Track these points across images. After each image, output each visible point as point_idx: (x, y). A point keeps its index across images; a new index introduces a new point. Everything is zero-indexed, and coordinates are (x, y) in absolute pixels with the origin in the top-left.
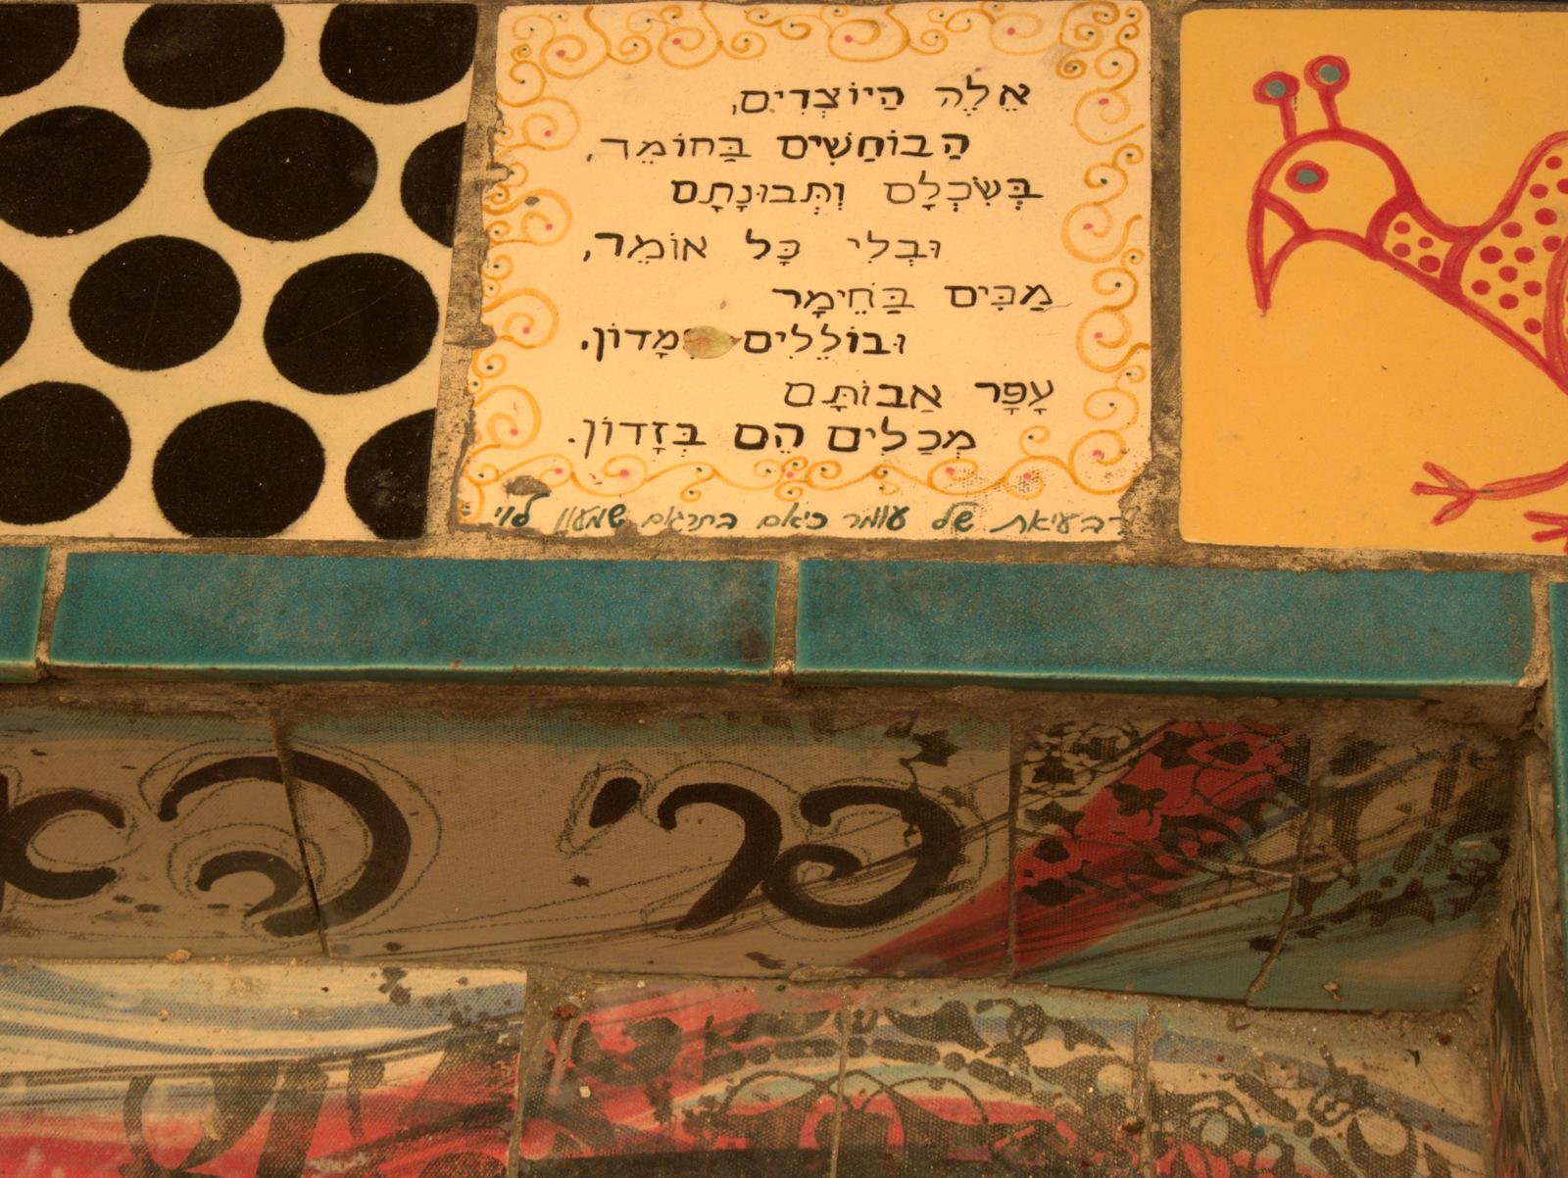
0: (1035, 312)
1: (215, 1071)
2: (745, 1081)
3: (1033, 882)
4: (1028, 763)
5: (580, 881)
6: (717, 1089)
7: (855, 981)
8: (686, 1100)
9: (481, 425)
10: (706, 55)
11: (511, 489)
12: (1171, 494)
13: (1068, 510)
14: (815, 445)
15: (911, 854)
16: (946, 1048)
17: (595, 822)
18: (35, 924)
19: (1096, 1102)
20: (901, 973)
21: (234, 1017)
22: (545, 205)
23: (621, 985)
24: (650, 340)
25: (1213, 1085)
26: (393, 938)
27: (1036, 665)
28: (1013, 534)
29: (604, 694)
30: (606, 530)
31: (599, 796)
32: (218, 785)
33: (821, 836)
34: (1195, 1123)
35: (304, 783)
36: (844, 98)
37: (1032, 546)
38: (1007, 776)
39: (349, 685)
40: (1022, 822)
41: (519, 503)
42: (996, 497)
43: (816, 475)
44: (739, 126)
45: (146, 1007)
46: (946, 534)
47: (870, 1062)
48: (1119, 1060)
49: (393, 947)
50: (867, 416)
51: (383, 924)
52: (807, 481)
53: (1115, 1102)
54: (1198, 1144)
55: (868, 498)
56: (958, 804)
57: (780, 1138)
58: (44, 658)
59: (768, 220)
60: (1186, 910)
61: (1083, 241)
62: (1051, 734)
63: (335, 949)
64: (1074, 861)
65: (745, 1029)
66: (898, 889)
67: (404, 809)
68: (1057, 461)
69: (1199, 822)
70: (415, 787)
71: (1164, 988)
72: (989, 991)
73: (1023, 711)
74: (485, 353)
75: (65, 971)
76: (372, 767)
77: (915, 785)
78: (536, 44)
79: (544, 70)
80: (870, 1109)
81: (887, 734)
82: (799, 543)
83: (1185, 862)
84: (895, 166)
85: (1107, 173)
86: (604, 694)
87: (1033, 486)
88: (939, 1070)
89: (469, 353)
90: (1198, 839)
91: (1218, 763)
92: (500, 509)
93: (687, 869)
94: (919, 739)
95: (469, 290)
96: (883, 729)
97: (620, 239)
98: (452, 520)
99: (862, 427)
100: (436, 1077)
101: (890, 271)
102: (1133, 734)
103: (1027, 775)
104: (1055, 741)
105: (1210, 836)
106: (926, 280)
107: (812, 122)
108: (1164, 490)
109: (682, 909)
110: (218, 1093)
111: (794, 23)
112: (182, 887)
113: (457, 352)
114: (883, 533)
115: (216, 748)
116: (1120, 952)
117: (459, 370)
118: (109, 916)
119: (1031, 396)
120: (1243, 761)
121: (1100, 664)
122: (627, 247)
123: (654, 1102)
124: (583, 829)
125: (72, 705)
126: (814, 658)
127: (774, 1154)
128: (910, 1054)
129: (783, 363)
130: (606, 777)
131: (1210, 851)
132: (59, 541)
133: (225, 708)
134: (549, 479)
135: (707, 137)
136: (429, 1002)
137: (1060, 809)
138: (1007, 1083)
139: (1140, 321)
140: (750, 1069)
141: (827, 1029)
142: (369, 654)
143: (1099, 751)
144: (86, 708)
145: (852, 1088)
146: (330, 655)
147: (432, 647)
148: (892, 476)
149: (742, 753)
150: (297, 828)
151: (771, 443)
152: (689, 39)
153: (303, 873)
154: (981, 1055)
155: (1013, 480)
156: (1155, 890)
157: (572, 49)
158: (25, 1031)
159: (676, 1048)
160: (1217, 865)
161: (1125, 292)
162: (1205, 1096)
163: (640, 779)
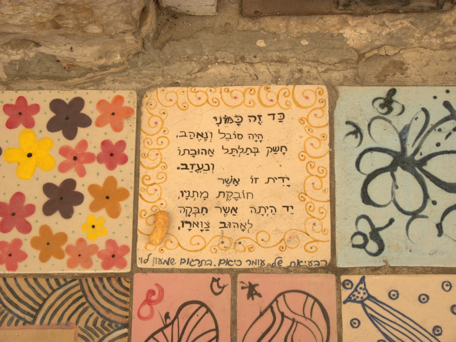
10: (310, 244)
38: (328, 156)
135: (220, 196)
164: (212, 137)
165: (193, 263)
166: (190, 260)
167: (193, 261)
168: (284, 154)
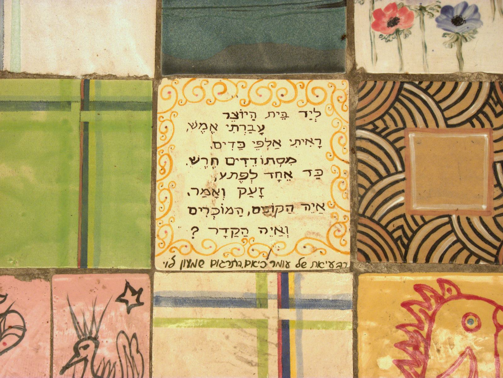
0: (204, 198)
36: (240, 115)
92: (250, 133)
99: (202, 207)
111: (315, 96)
164: (233, 147)
165: (222, 265)
166: (220, 262)
167: (223, 262)
168: (279, 181)
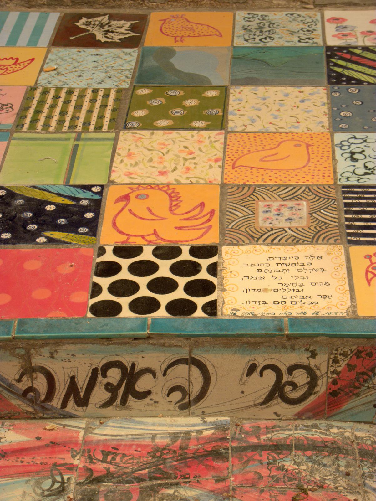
1: (169, 434)
2: (275, 435)
3: (331, 391)
4: (331, 358)
5: (243, 392)
6: (269, 436)
7: (295, 419)
8: (263, 438)
9: (226, 301)
11: (232, 310)
12: (356, 309)
13: (337, 312)
14: (288, 303)
15: (308, 383)
16: (314, 430)
17: (247, 376)
18: (133, 407)
19: (345, 437)
20: (304, 418)
21: (172, 425)
22: (234, 273)
23: (248, 421)
24: (256, 290)
25: (367, 435)
26: (203, 410)
27: (333, 332)
28: (327, 315)
29: (252, 340)
30: (251, 315)
31: (249, 368)
32: (176, 366)
33: (291, 379)
34: (364, 441)
35: (192, 365)
37: (330, 316)
38: (327, 362)
39: (205, 338)
40: (329, 375)
41: (234, 312)
42: (323, 310)
43: (289, 308)
44: (269, 262)
45: (154, 424)
46: (315, 315)
47: (299, 432)
48: (348, 432)
49: (203, 412)
50: (298, 300)
51: (203, 405)
52: (288, 308)
53: (348, 438)
54: (366, 444)
55: (300, 311)
56: (317, 369)
57: (283, 443)
58: (149, 332)
59: (275, 274)
60: (361, 397)
61: (335, 276)
62: (335, 350)
63: (191, 413)
64: (339, 386)
65: (274, 427)
66: (304, 394)
67: (211, 372)
68: (334, 305)
69: (363, 373)
70: (213, 366)
71: (356, 420)
72: (321, 421)
73: (330, 344)
74: (225, 293)
75: (137, 419)
76: (206, 361)
77: (309, 364)
78: (229, 251)
79: (231, 255)
80: (300, 438)
81: (305, 350)
82: (287, 317)
83: (360, 384)
84: (297, 267)
85: (338, 268)
86: (252, 340)
87: (330, 309)
88: (313, 433)
89: (222, 292)
90: (363, 378)
91: (367, 357)
93: (264, 388)
94: (311, 351)
95: (221, 284)
96: (304, 349)
97: (248, 277)
98: (222, 314)
100: (213, 434)
101: (299, 281)
102: (351, 350)
103: (331, 361)
104: (336, 352)
105: (366, 377)
106: (306, 282)
107: (282, 261)
108: (354, 309)
109: (262, 400)
110: (170, 437)
112: (164, 396)
113: (220, 292)
114: (303, 315)
115: (177, 356)
116: (348, 410)
117: (221, 294)
118: (148, 405)
119: (328, 297)
120: (371, 357)
121: (346, 332)
122: (250, 278)
123: (257, 438)
124: (245, 378)
125: (152, 344)
126: (292, 331)
127: (282, 445)
128: (307, 431)
129: (281, 293)
130: (251, 363)
131: (365, 381)
132: (149, 317)
133: (181, 344)
134: (239, 309)
136: (211, 422)
137: (337, 371)
138: (327, 435)
139: (347, 287)
140: (275, 433)
141: (290, 427)
142: (209, 331)
143: (344, 354)
144: (154, 345)
145: (296, 435)
146: (202, 332)
147: (221, 330)
148: (303, 308)
149: (277, 356)
150: (189, 378)
151: (280, 303)
152: (258, 251)
153: (188, 392)
154: (321, 431)
155: (326, 308)
156: (355, 392)
157: (236, 252)
158: (130, 428)
159: (260, 430)
160: (366, 385)
161: (344, 283)
162: (366, 437)
163: (257, 363)
